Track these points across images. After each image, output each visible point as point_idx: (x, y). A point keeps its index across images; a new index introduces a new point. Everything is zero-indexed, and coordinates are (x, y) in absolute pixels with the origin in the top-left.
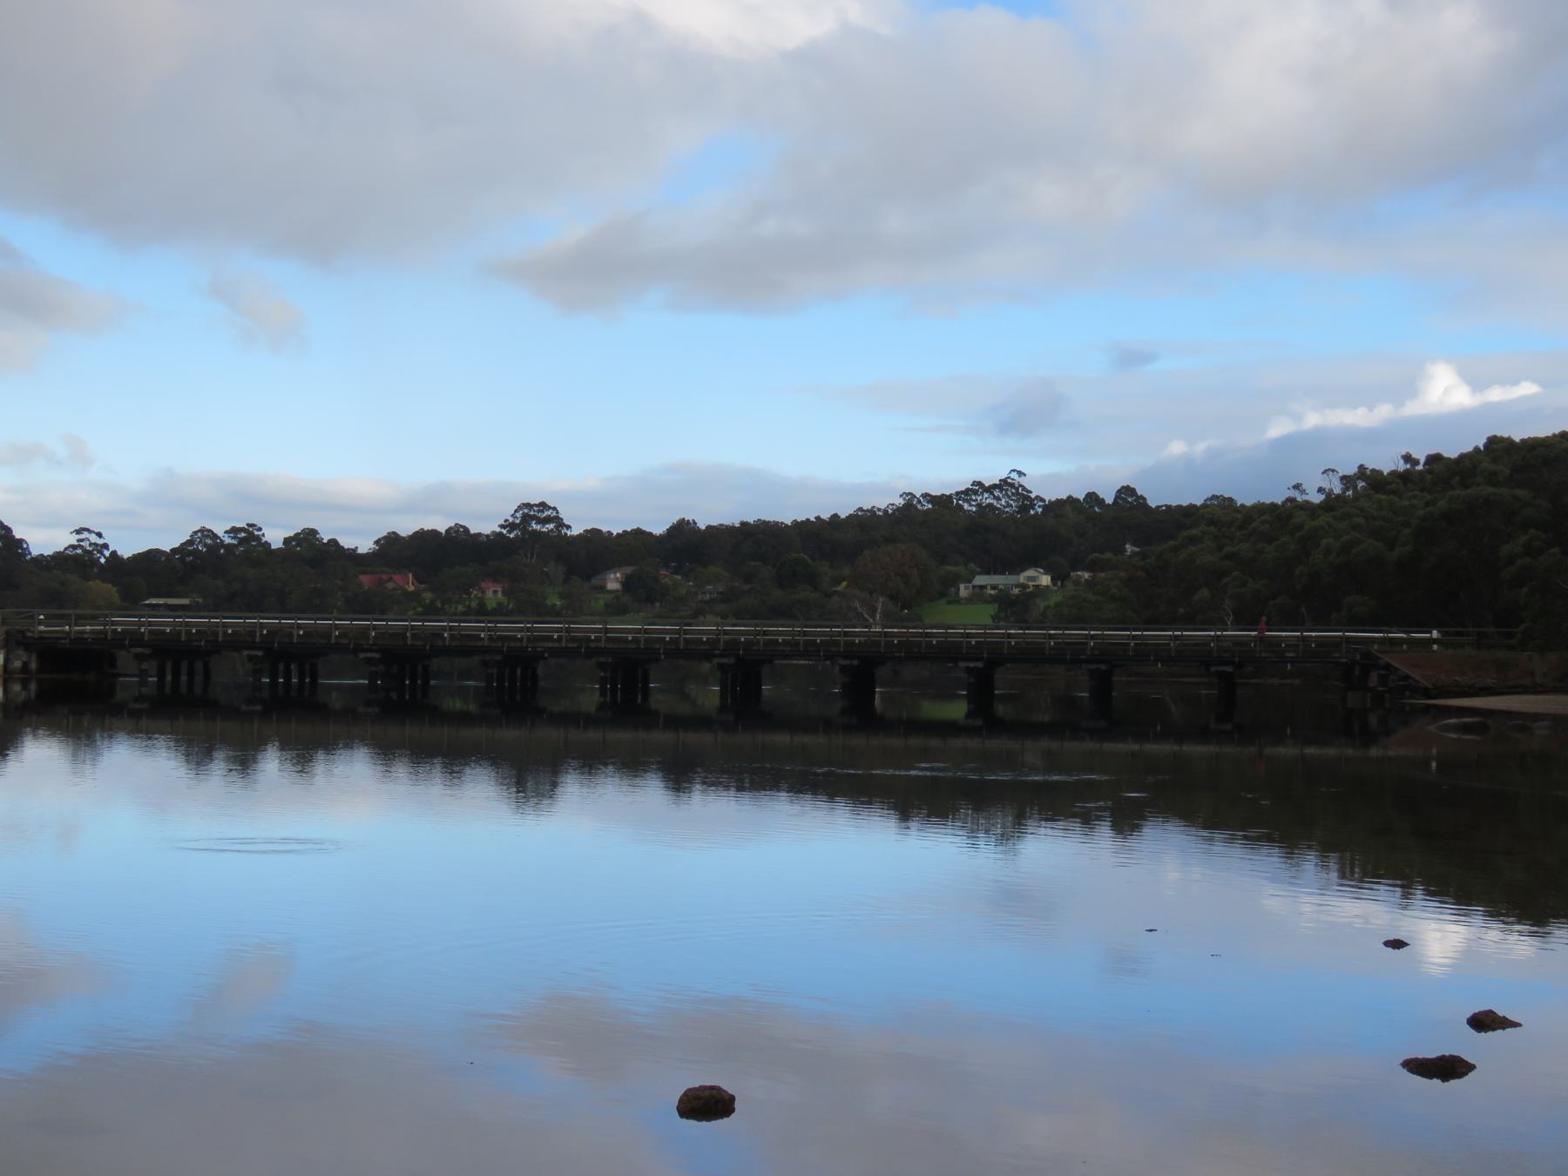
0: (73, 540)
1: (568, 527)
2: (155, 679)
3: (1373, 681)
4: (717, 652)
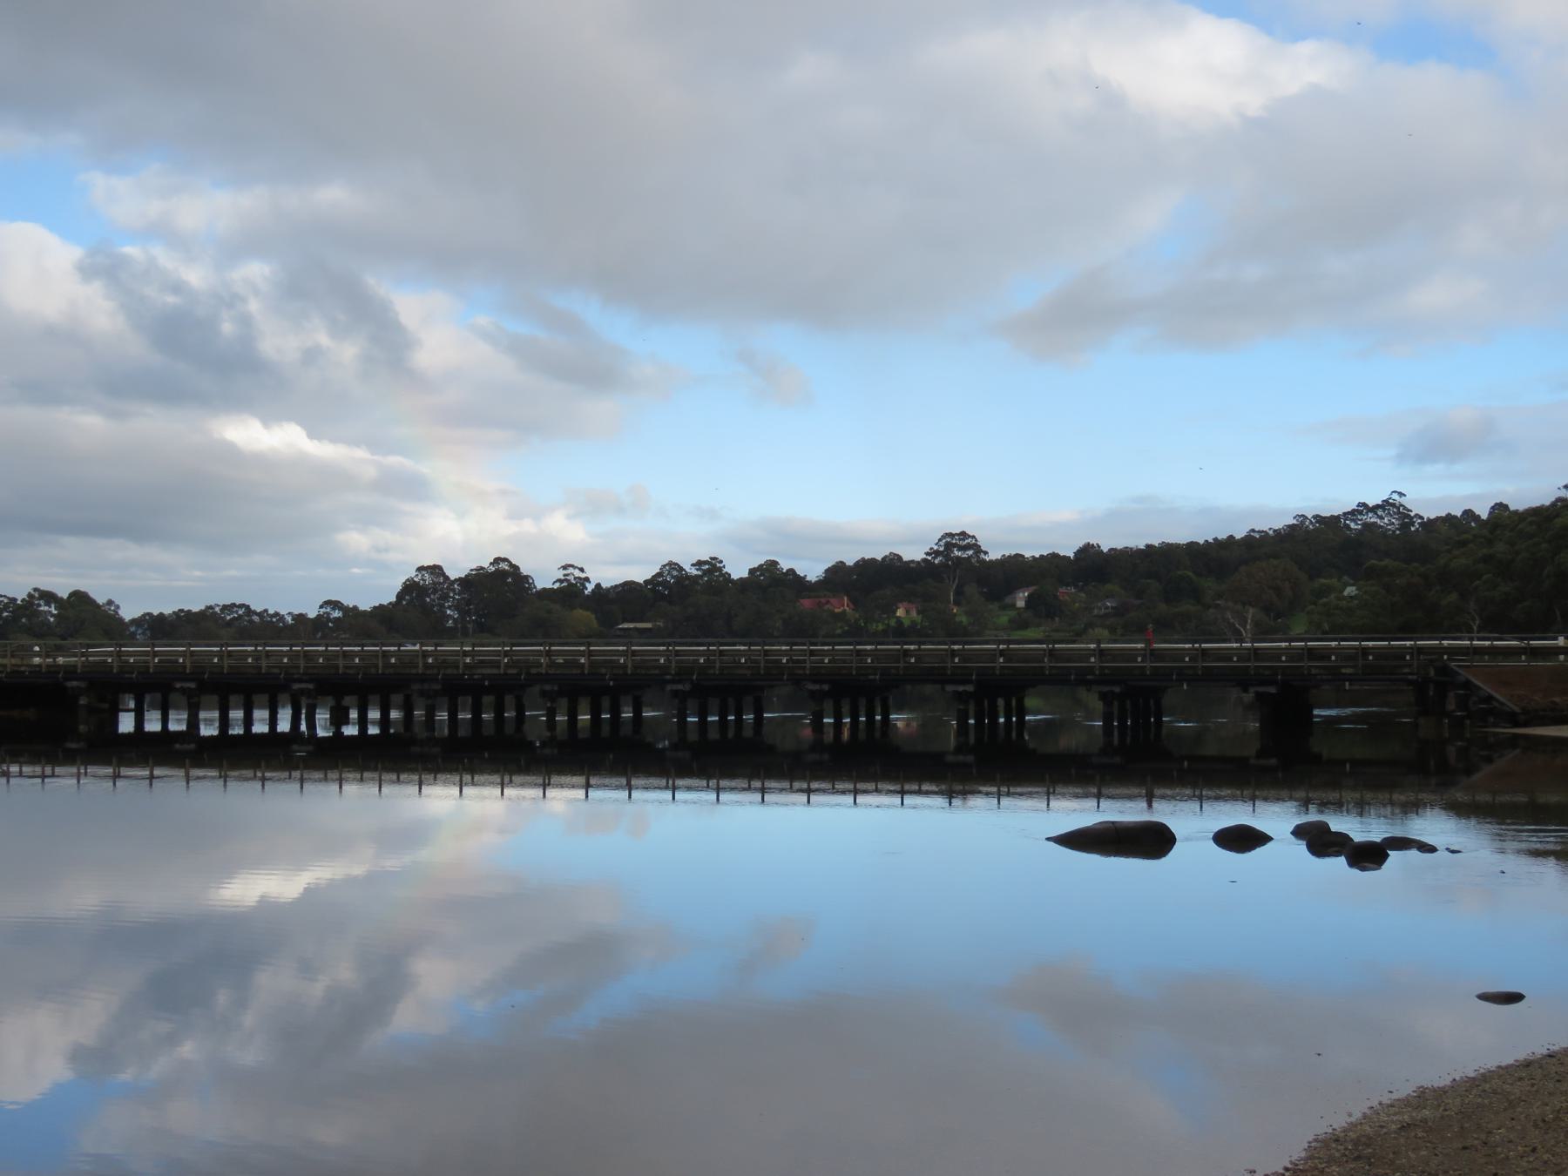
0: (560, 575)
1: (986, 553)
2: (825, 720)
3: (1451, 705)
4: (668, 677)
